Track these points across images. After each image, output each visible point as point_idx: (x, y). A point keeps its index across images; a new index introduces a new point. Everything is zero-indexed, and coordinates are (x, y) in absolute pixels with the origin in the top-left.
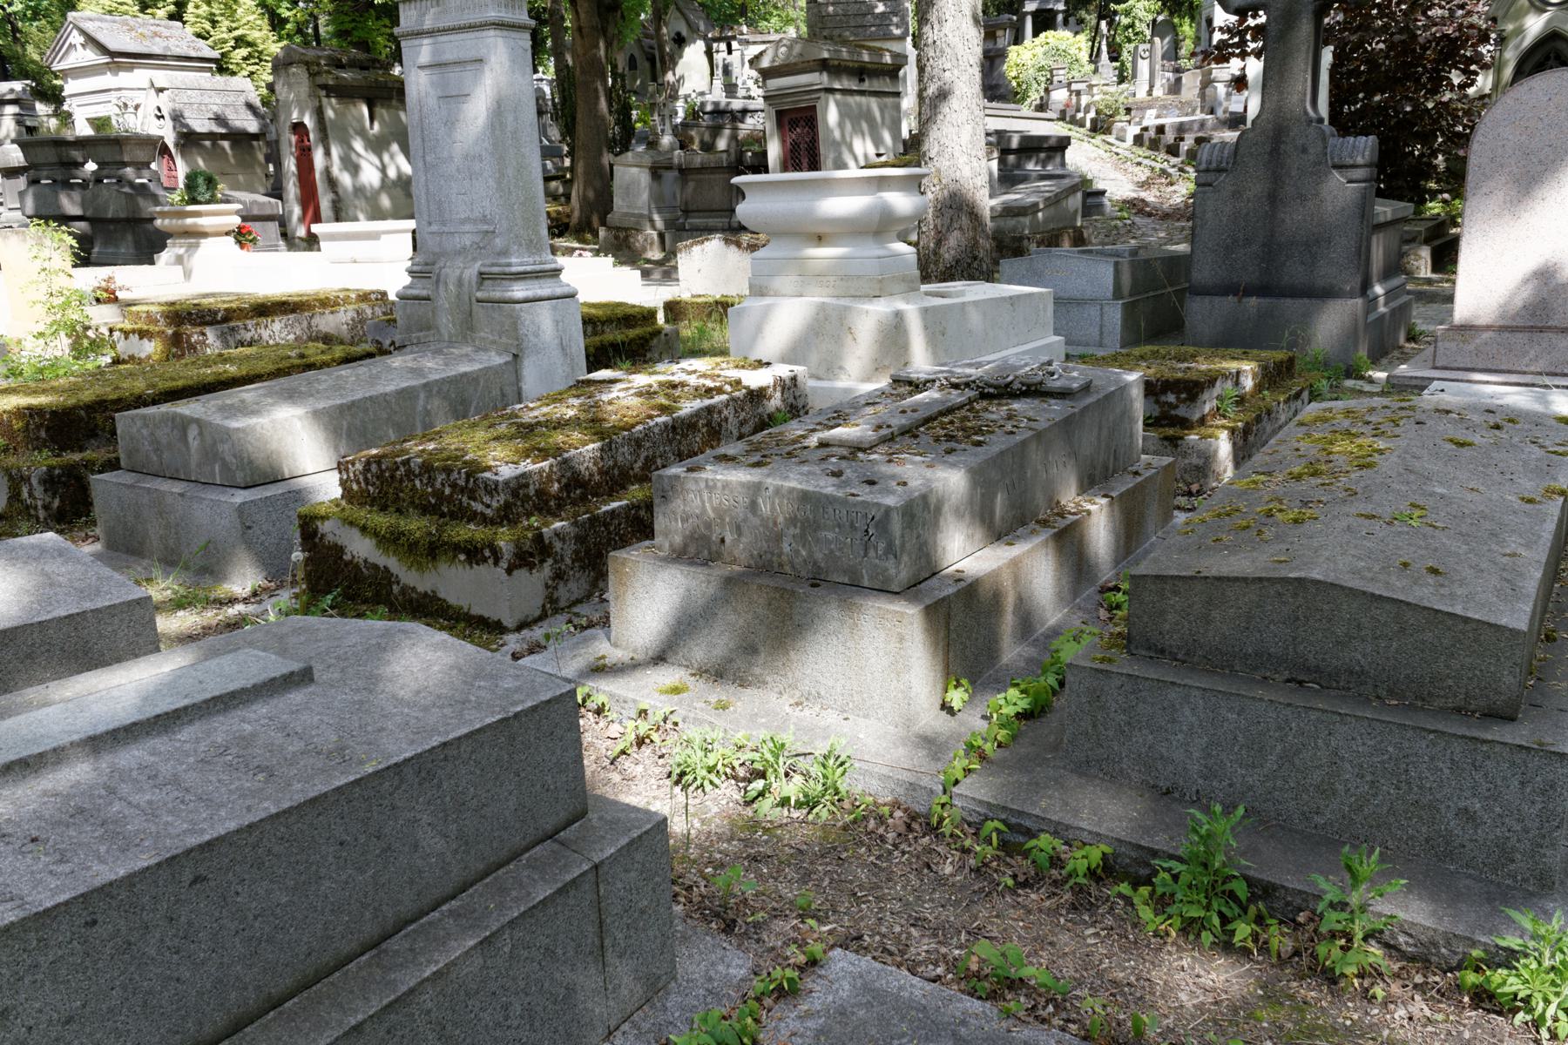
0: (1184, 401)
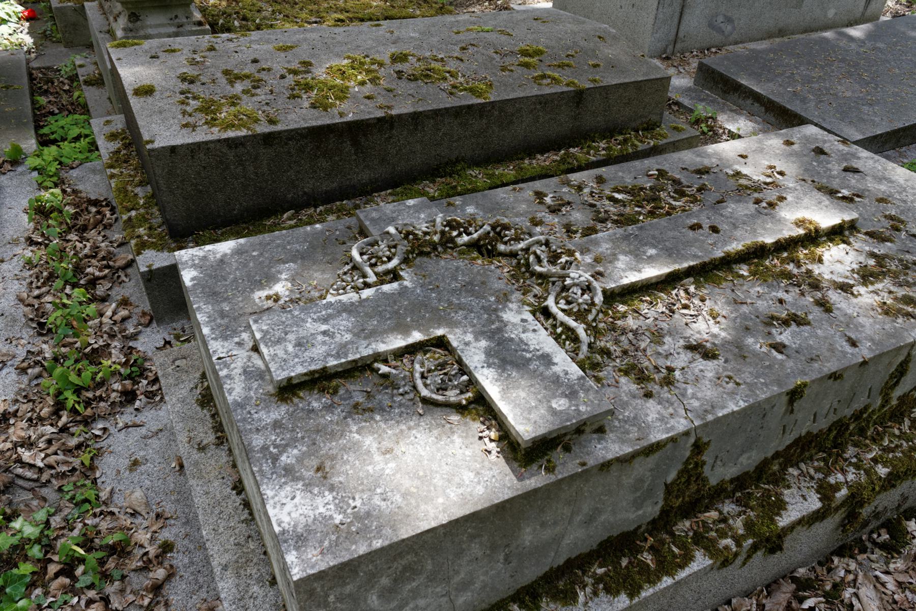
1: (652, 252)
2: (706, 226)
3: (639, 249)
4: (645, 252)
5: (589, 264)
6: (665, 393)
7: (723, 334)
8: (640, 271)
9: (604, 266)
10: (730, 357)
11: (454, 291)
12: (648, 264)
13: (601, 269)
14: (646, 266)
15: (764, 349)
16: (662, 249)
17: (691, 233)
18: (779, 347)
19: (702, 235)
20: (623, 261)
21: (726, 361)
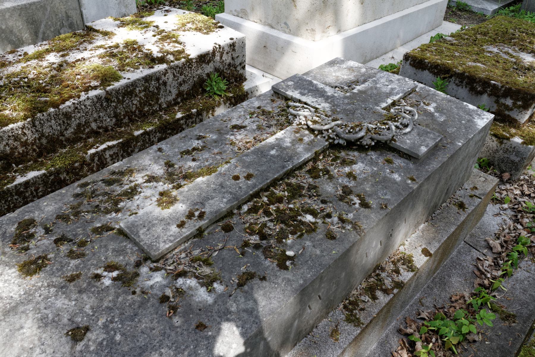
0: (519, 107)
1: (273, 152)
2: (242, 179)
3: (281, 153)
4: (277, 151)
5: (304, 136)
6: (252, 110)
7: (228, 136)
8: (277, 139)
9: (297, 137)
10: (225, 129)
11: (357, 109)
12: (273, 144)
13: (297, 135)
14: (274, 143)
15: (208, 135)
16: (267, 155)
17: (251, 171)
18: (199, 138)
19: (244, 172)
20: (287, 143)
21: (227, 127)
